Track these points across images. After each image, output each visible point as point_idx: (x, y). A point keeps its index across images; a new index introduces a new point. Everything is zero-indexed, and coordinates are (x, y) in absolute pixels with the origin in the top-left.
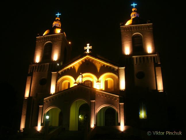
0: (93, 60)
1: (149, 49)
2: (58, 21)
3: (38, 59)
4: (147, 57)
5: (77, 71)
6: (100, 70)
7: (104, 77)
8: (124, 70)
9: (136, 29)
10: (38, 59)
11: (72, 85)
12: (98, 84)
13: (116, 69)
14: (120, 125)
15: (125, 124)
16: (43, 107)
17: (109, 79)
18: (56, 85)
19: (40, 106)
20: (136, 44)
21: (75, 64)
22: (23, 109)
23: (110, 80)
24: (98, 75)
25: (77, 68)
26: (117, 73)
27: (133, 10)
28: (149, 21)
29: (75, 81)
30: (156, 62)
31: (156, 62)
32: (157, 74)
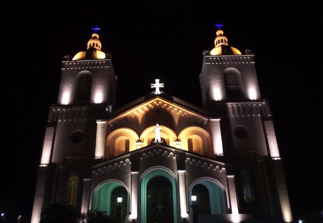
1: (253, 93)
2: (96, 39)
3: (66, 98)
5: (140, 121)
7: (185, 134)
8: (219, 122)
10: (66, 98)
11: (134, 147)
12: (177, 144)
14: (231, 213)
15: (240, 212)
16: (138, 176)
18: (105, 143)
24: (177, 132)
26: (207, 128)
28: (249, 51)
29: (139, 137)
32: (267, 132)
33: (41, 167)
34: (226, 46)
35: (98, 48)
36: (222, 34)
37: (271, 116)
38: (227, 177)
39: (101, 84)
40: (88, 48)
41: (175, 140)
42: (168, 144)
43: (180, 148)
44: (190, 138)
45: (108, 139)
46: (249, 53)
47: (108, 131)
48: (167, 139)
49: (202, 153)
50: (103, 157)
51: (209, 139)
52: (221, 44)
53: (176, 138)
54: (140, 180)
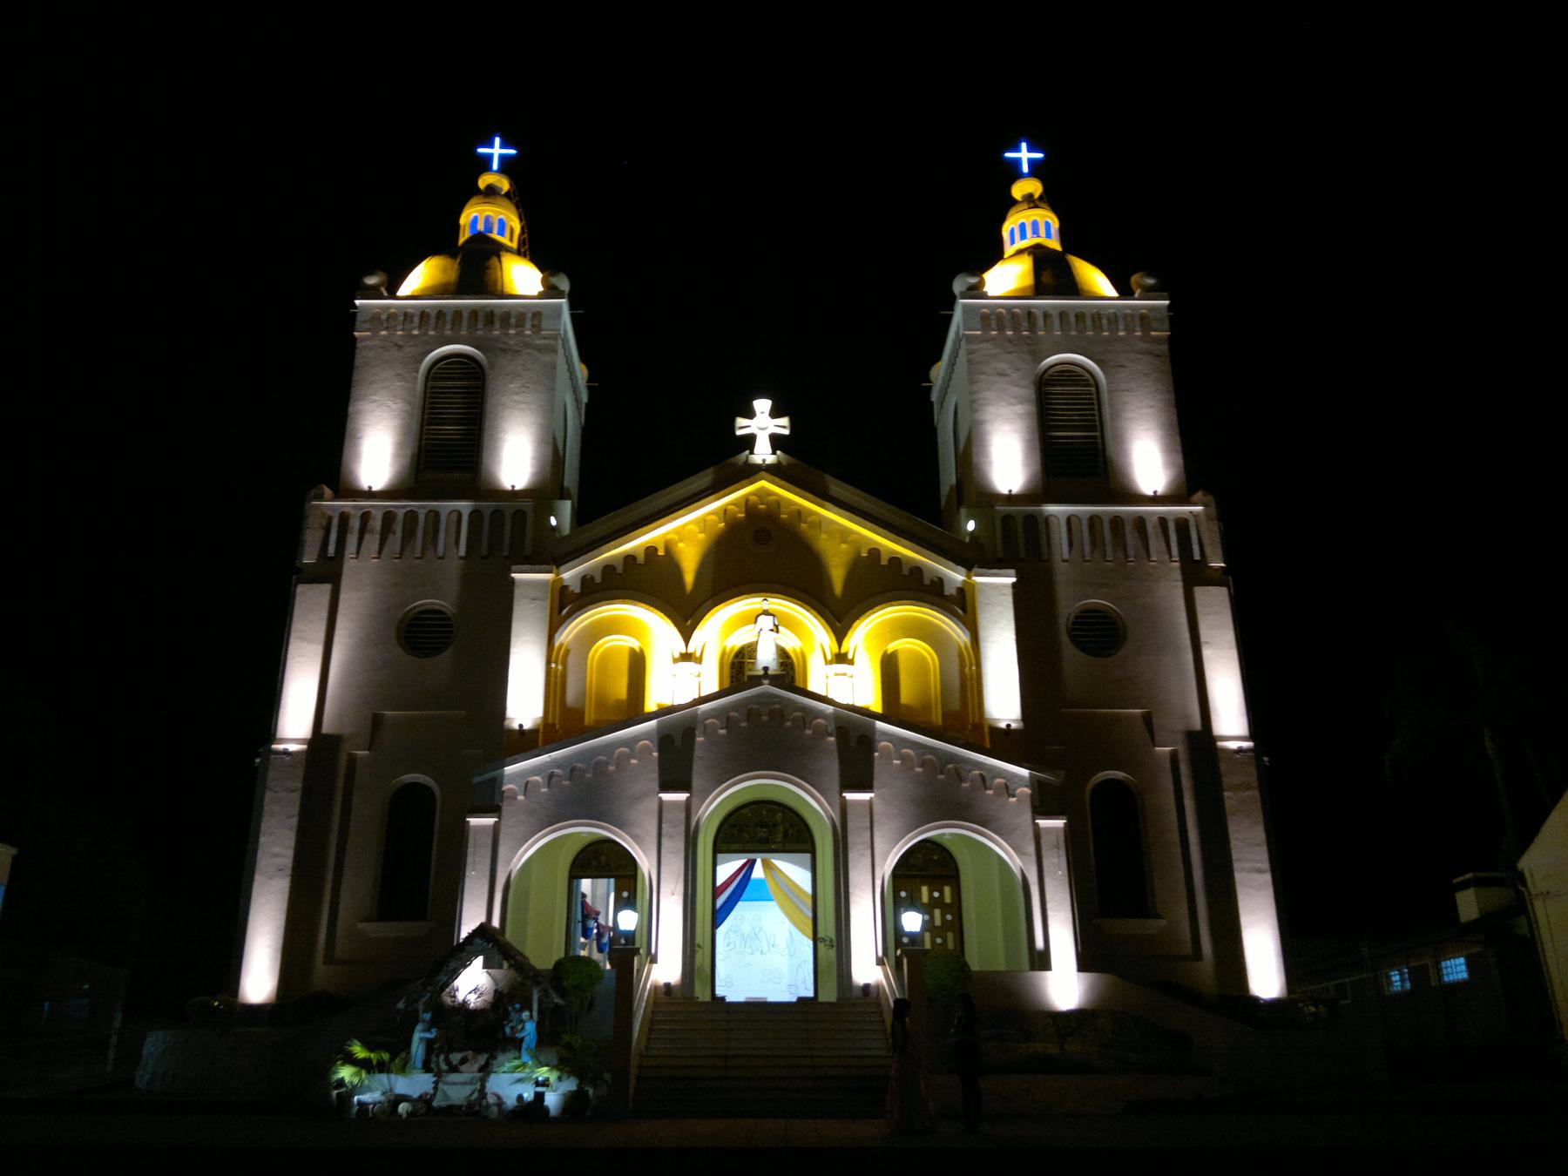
0: (800, 514)
4: (1140, 522)
5: (689, 578)
6: (849, 579)
8: (1009, 591)
9: (1062, 329)
13: (953, 581)
15: (1083, 965)
17: (906, 646)
19: (474, 821)
20: (1059, 428)
21: (676, 531)
22: (264, 826)
23: (920, 662)
24: (840, 618)
25: (689, 561)
27: (1022, 189)
28: (1150, 281)
30: (1197, 557)
31: (1197, 557)
33: (278, 753)
34: (1054, 251)
35: (504, 240)
36: (1037, 196)
37: (1223, 565)
38: (1037, 824)
39: (523, 406)
40: (462, 240)
41: (829, 657)
42: (799, 684)
43: (851, 703)
44: (890, 651)
45: (557, 644)
46: (1149, 292)
47: (560, 612)
48: (799, 651)
49: (937, 718)
50: (540, 725)
51: (965, 654)
52: (1030, 241)
53: (836, 649)
54: (691, 833)
